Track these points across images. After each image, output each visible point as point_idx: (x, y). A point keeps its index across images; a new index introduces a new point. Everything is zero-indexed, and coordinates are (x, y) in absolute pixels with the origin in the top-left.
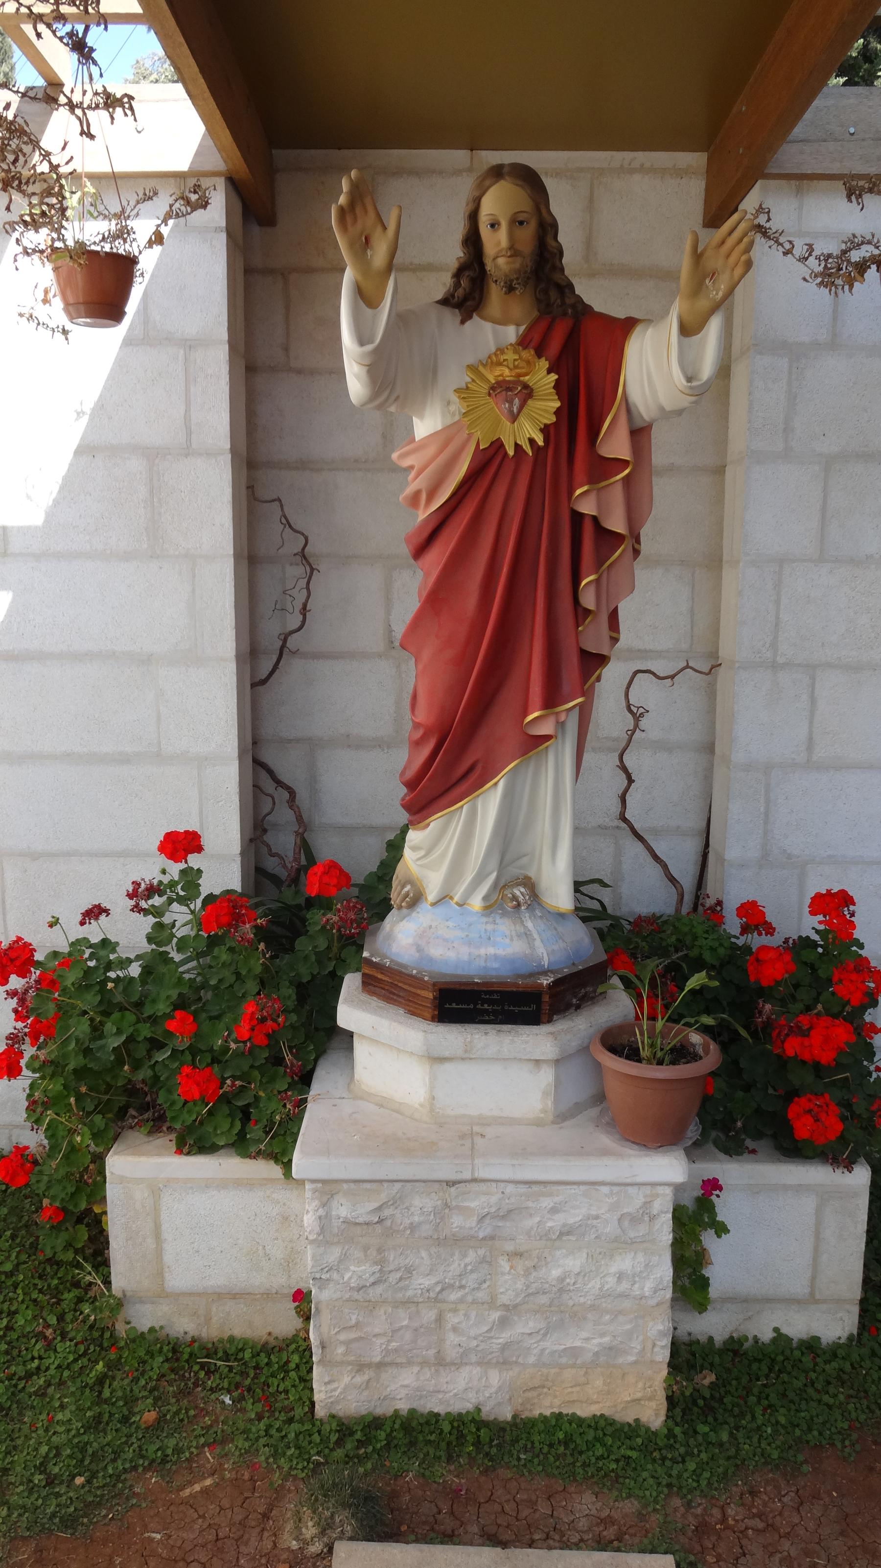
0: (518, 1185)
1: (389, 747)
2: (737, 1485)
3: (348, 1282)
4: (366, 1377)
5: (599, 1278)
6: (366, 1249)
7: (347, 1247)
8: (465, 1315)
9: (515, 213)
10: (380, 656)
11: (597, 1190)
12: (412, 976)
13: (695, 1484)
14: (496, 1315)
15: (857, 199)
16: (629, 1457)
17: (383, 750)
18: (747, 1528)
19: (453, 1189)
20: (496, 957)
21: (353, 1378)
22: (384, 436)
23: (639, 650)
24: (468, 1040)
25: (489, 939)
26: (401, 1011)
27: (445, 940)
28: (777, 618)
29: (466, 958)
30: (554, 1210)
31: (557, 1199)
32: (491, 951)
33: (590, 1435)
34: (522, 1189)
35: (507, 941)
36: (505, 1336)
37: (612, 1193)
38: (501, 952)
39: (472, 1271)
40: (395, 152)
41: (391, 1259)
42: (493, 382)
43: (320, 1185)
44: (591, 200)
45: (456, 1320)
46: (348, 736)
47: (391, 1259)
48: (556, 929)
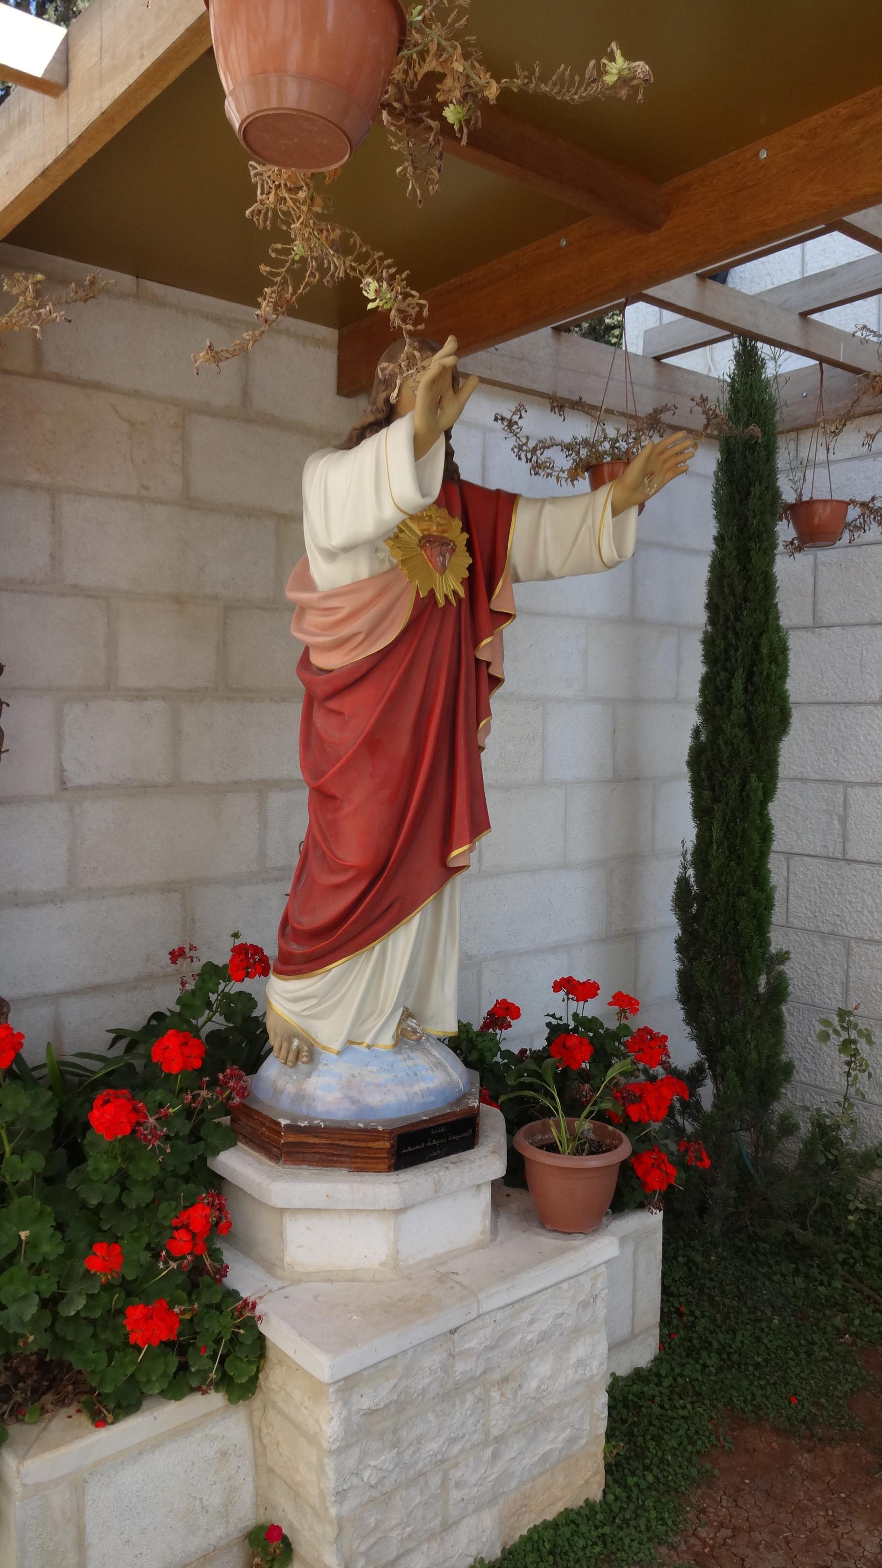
1: (62, 901)
2: (688, 1512)
3: (368, 1482)
7: (365, 1443)
10: (50, 799)
12: (360, 1130)
13: (664, 1528)
14: (488, 1453)
15: (559, 412)
16: (603, 1535)
17: (56, 905)
18: (724, 1540)
19: (456, 1335)
22: (52, 556)
24: (437, 1178)
26: (344, 1172)
27: (378, 1086)
29: (405, 1098)
30: (531, 1322)
31: (533, 1310)
32: (423, 1086)
33: (567, 1531)
34: (508, 1311)
35: (430, 1072)
36: (498, 1468)
38: (431, 1085)
39: (470, 1415)
42: (421, 535)
43: (342, 1383)
45: (459, 1474)
46: (16, 893)
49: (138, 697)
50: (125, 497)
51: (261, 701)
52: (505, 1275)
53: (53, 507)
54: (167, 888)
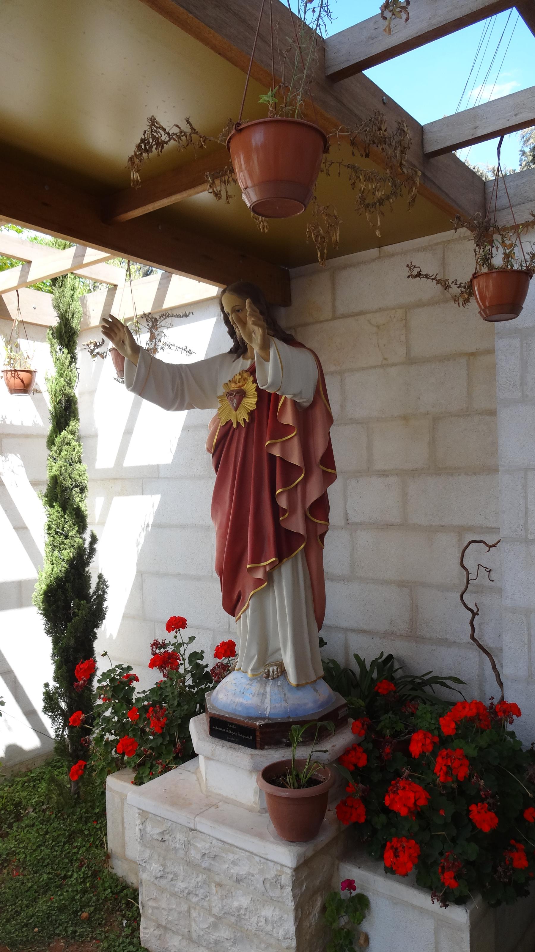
0: (218, 841)
1: (348, 581)
4: (160, 932)
5: (257, 917)
6: (159, 856)
7: (152, 852)
8: (199, 913)
9: (233, 307)
11: (254, 858)
14: (212, 920)
19: (191, 833)
20: (241, 704)
21: (154, 930)
22: (341, 406)
23: (487, 528)
25: (243, 693)
28: (526, 508)
31: (236, 857)
32: (241, 700)
34: (220, 844)
35: (251, 696)
37: (260, 863)
38: (245, 702)
40: (343, 257)
41: (169, 865)
44: (444, 259)
47: (169, 865)
48: (285, 694)
49: (383, 475)
50: (375, 367)
51: (459, 475)
52: (250, 831)
53: (342, 381)
54: (401, 584)
